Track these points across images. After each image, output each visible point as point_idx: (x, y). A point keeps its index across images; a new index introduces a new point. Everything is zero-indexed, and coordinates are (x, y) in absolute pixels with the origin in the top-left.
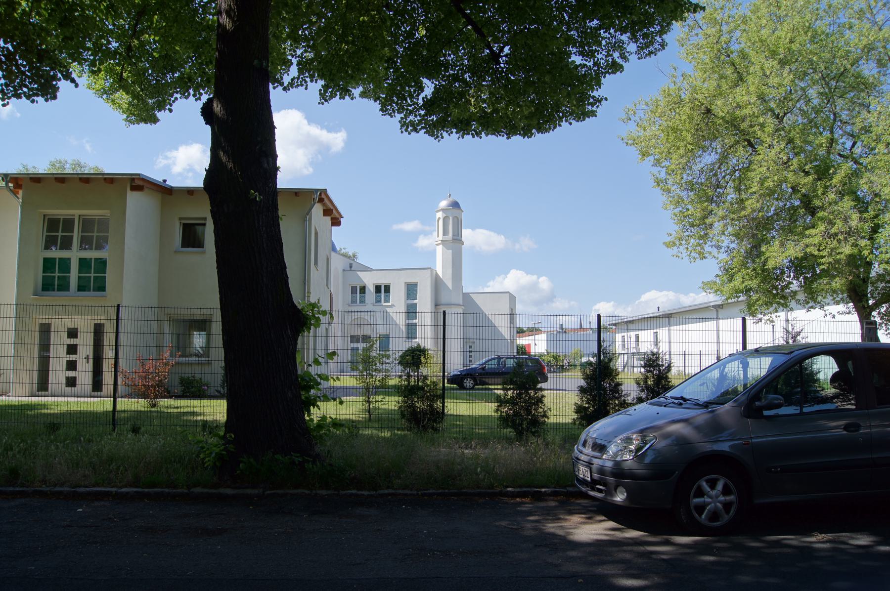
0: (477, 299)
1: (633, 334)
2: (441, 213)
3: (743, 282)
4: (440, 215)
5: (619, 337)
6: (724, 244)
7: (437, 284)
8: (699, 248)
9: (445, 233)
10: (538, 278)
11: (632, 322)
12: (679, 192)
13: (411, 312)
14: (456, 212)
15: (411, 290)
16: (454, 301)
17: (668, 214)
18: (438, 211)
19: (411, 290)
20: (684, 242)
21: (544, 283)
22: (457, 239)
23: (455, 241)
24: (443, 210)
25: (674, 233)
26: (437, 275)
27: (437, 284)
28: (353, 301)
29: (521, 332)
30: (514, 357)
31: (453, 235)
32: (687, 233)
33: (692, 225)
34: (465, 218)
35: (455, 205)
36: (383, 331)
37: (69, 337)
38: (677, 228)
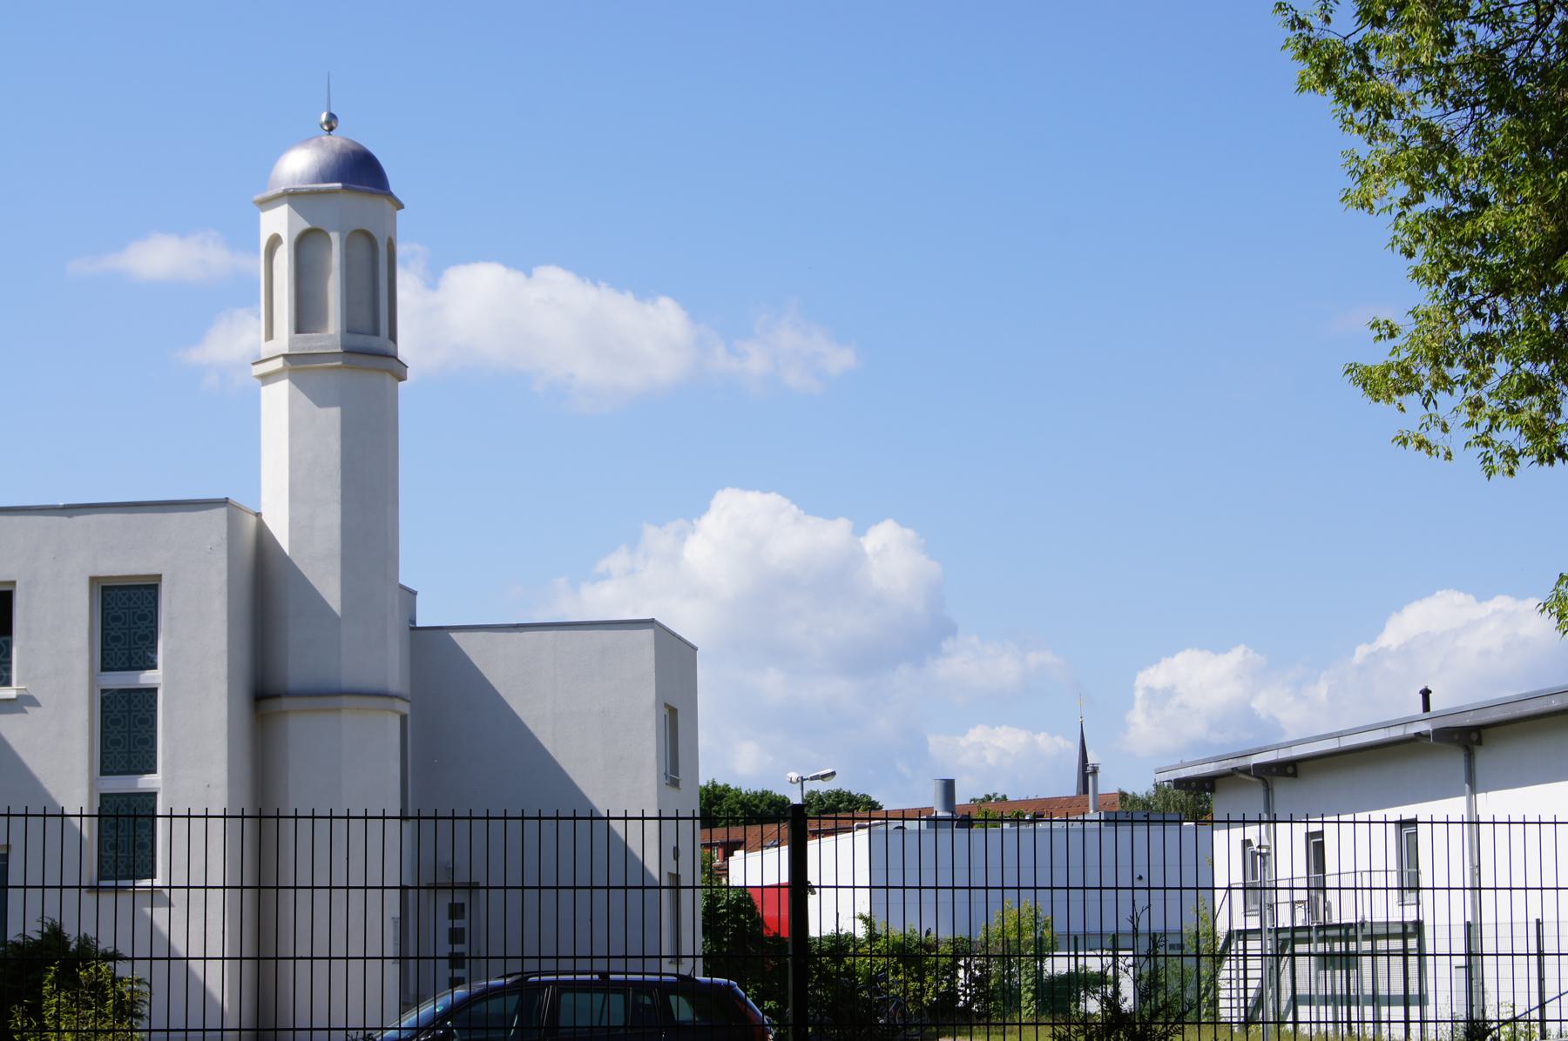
0: (495, 663)
4: (279, 222)
7: (264, 581)
8: (1533, 406)
10: (860, 530)
11: (1289, 769)
12: (1427, 109)
13: (126, 730)
14: (361, 208)
15: (127, 618)
16: (353, 671)
17: (1380, 228)
18: (268, 203)
19: (127, 618)
20: (1457, 371)
21: (890, 554)
22: (370, 348)
23: (357, 353)
24: (292, 197)
25: (1407, 325)
26: (263, 538)
27: (264, 581)
29: (732, 815)
31: (349, 329)
32: (1474, 327)
33: (1501, 286)
35: (360, 171)
38: (1424, 297)
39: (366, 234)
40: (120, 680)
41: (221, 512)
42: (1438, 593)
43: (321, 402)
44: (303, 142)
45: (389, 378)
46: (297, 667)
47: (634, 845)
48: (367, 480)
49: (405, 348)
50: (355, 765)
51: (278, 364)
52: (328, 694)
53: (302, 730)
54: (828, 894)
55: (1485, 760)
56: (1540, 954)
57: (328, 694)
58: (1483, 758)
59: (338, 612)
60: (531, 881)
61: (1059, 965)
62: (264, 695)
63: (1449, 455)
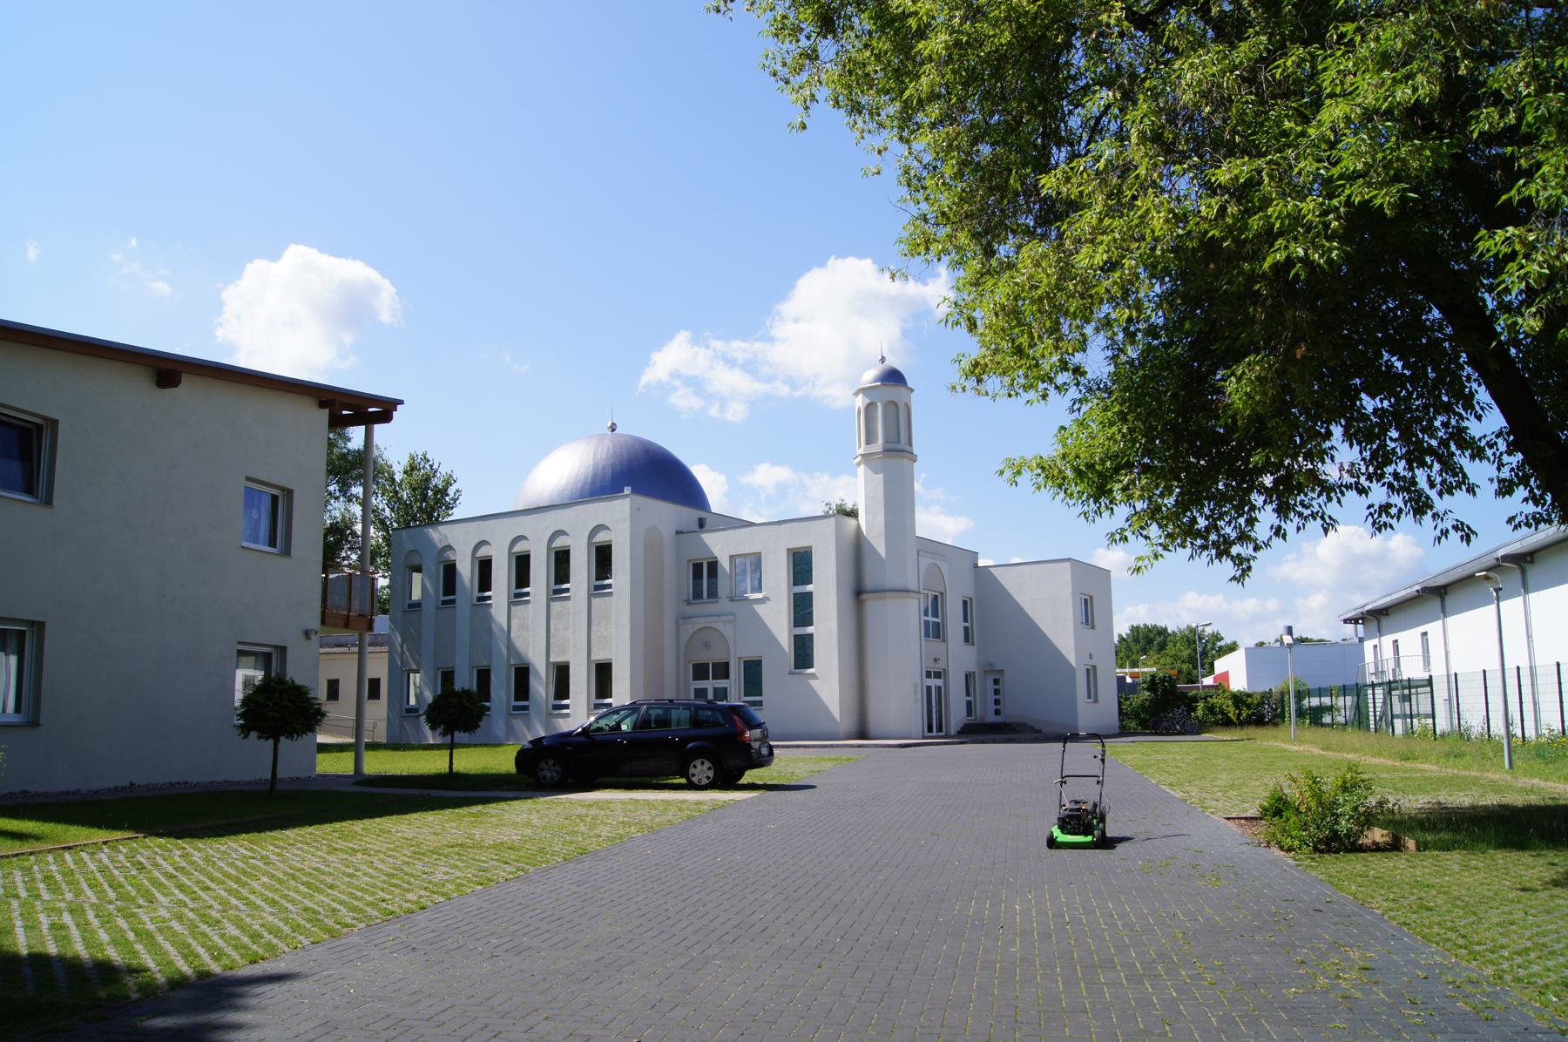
0: (1007, 580)
1: (1387, 640)
6: (1129, 348)
9: (870, 439)
13: (802, 610)
14: (893, 392)
15: (801, 565)
16: (892, 580)
19: (801, 565)
28: (697, 595)
30: (687, 707)
31: (886, 441)
36: (750, 654)
37: (695, 678)
39: (895, 404)
40: (800, 589)
42: (832, 262)
43: (876, 472)
45: (906, 461)
46: (870, 582)
48: (898, 502)
52: (880, 591)
53: (872, 605)
55: (1450, 600)
57: (880, 591)
58: (1449, 600)
61: (1315, 702)
62: (859, 592)
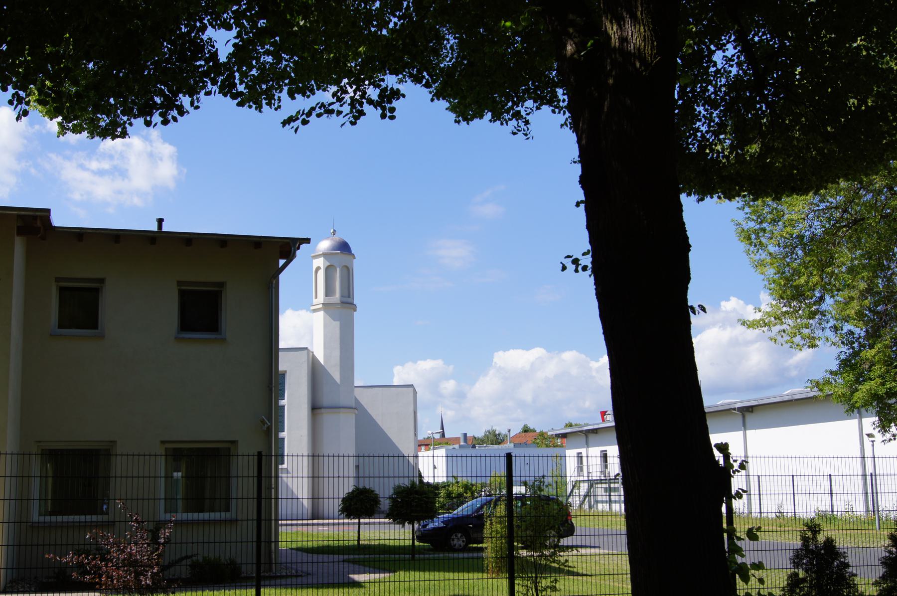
2: (321, 259)
3: (883, 384)
4: (320, 262)
5: (571, 454)
7: (316, 372)
9: (328, 292)
14: (344, 258)
24: (325, 255)
26: (314, 356)
27: (316, 372)
31: (342, 296)
34: (358, 266)
35: (344, 247)
41: (306, 352)
44: (327, 238)
47: (290, 484)
49: (356, 301)
50: (343, 438)
51: (321, 306)
52: (336, 408)
53: (327, 418)
54: (118, 480)
56: (831, 494)
59: (338, 381)
60: (376, 475)
63: (704, 310)
